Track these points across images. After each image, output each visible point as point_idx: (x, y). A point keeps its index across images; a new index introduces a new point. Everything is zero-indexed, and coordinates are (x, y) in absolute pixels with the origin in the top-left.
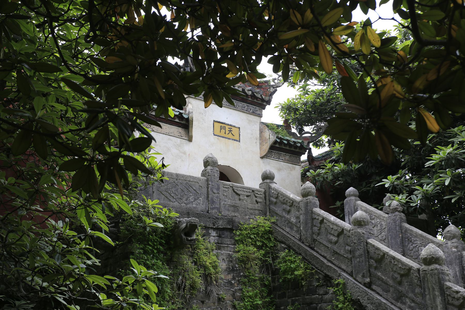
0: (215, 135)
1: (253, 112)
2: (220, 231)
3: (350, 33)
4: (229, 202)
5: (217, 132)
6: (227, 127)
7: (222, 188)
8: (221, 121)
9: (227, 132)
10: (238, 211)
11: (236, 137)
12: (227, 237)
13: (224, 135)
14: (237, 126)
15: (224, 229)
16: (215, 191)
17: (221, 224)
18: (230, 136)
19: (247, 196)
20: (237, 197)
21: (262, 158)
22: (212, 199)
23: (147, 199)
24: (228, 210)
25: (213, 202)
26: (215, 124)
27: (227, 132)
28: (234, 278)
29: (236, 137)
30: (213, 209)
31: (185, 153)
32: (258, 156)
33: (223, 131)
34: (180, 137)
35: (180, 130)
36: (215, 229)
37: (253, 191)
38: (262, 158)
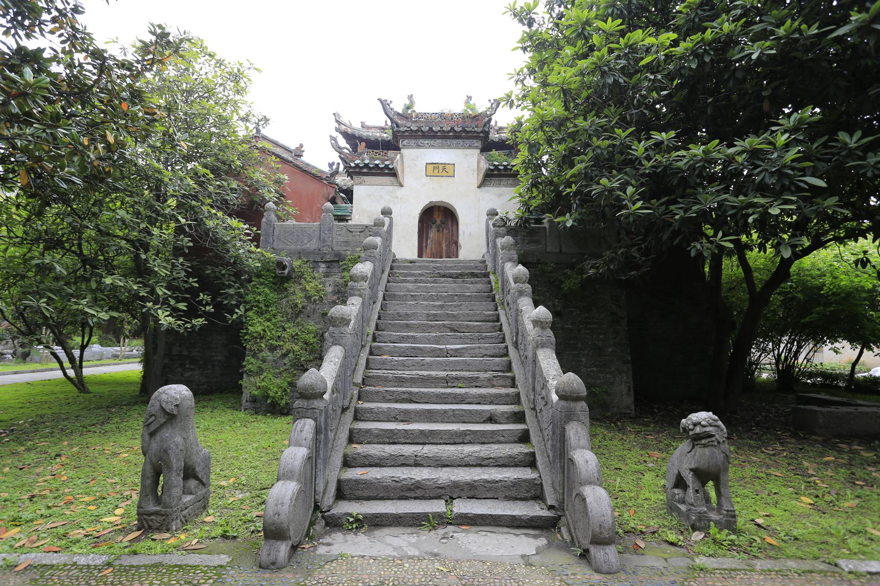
0: (427, 176)
1: (470, 146)
2: (330, 263)
3: (753, 25)
4: (341, 239)
5: (430, 172)
6: (441, 167)
7: (335, 228)
8: (434, 162)
9: (441, 170)
10: (350, 246)
11: (451, 174)
12: (334, 268)
13: (438, 174)
14: (451, 163)
15: (331, 261)
16: (326, 232)
17: (328, 258)
18: (444, 173)
19: (360, 232)
20: (350, 234)
21: (479, 187)
22: (324, 239)
23: (780, 209)
24: (341, 246)
25: (324, 241)
26: (428, 166)
27: (441, 170)
28: (338, 298)
29: (451, 174)
30: (324, 246)
31: (397, 197)
32: (476, 185)
33: (436, 170)
34: (393, 185)
35: (392, 178)
36: (324, 262)
37: (367, 227)
38: (479, 187)
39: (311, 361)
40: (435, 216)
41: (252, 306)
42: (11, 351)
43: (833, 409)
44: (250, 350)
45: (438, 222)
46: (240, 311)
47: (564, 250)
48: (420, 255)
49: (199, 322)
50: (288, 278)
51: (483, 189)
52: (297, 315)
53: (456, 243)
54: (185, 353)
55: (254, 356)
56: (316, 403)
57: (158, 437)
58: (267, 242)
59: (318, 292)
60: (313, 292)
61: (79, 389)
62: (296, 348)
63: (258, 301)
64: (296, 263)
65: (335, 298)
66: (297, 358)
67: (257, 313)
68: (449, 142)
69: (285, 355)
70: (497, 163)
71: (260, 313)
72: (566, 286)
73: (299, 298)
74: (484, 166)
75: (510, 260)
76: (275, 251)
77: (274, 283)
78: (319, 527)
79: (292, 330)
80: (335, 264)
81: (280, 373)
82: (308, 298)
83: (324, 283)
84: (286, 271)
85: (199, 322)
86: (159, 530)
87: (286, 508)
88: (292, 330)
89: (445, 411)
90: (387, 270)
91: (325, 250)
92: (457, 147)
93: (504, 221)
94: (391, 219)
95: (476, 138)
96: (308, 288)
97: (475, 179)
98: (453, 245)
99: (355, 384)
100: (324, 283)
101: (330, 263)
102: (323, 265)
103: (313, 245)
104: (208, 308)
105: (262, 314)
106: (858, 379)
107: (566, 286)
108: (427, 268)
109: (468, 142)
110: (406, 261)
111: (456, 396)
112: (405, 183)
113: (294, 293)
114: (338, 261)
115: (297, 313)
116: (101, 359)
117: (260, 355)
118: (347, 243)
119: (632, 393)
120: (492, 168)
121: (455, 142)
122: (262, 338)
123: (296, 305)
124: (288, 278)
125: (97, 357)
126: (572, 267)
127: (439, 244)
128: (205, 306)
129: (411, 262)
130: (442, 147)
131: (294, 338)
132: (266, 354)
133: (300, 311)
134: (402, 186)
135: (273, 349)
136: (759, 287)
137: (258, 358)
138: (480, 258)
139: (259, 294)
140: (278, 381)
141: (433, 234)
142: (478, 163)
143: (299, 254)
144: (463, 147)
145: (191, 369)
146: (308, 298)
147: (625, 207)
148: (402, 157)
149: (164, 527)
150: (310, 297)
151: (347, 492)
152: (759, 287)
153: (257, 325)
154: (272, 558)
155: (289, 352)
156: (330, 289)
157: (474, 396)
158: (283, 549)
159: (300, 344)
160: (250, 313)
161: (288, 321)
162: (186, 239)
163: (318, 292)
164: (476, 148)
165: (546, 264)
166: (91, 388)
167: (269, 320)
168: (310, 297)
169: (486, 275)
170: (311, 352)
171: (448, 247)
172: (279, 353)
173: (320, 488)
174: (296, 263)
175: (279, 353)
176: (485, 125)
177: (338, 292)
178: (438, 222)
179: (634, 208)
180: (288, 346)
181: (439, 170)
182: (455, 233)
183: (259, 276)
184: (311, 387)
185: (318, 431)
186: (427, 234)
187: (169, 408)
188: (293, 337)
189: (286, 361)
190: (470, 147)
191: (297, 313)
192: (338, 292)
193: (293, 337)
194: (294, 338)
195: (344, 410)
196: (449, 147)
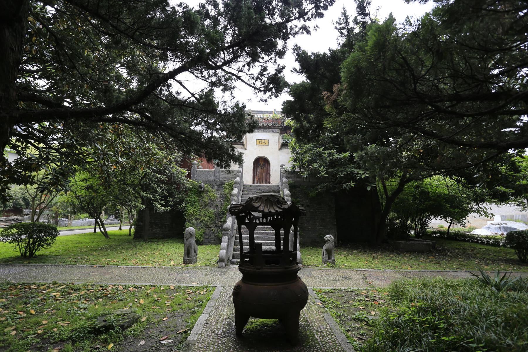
2: (219, 186)
4: (223, 176)
7: (221, 172)
17: (218, 183)
21: (279, 150)
32: (278, 149)
33: (261, 143)
35: (241, 146)
38: (279, 150)
39: (211, 224)
40: (260, 162)
41: (188, 203)
42: (47, 221)
43: (417, 242)
44: (188, 220)
45: (262, 165)
46: (184, 204)
47: (311, 181)
48: (253, 183)
49: (169, 208)
50: (203, 192)
51: (281, 151)
52: (206, 206)
53: (269, 174)
54: (153, 221)
55: (189, 222)
56: (228, 232)
57: (188, 240)
58: (194, 177)
59: (214, 197)
60: (212, 197)
61: (106, 237)
62: (206, 219)
63: (191, 201)
64: (206, 186)
65: (221, 199)
66: (206, 223)
67: (190, 205)
68: (266, 130)
69: (201, 222)
70: (286, 140)
71: (192, 205)
72: (310, 195)
73: (207, 200)
74: (281, 141)
75: (286, 188)
76: (197, 180)
77: (197, 193)
78: (229, 263)
79: (204, 212)
80: (221, 186)
81: (199, 229)
82: (210, 199)
83: (216, 194)
84: (202, 189)
85: (169, 208)
86: (189, 263)
87: (224, 255)
88: (204, 212)
89: (262, 237)
90: (242, 189)
91: (217, 180)
92: (270, 132)
93: (286, 171)
94: (243, 168)
95: (278, 128)
96: (210, 195)
97: (277, 146)
98: (268, 181)
99: (235, 230)
100: (216, 194)
101: (219, 186)
102: (216, 186)
103: (212, 178)
104: (171, 203)
105: (192, 205)
106: (428, 232)
107: (310, 195)
108: (257, 189)
109: (274, 130)
110: (249, 185)
111: (266, 233)
112: (247, 148)
113: (205, 198)
114: (222, 185)
115: (206, 205)
116: (90, 225)
117: (191, 222)
118: (225, 177)
119: (336, 237)
120: (285, 142)
121: (269, 130)
122: (192, 215)
123: (206, 202)
124: (203, 192)
125: (89, 224)
126: (313, 187)
127: (262, 174)
128: (170, 202)
129: (251, 186)
130: (263, 132)
131: (205, 215)
132: (194, 221)
133: (207, 205)
134: (246, 149)
135: (196, 219)
136: (390, 194)
137: (190, 223)
138: (278, 184)
139: (191, 198)
140: (199, 232)
141: (259, 170)
142: (279, 139)
143: (206, 182)
144: (272, 132)
145: (156, 228)
146: (210, 199)
147: (320, 173)
148: (246, 137)
149: (190, 263)
150: (211, 199)
151: (235, 257)
152: (390, 194)
153: (191, 210)
154: (221, 266)
155: (203, 220)
156: (219, 196)
157: (271, 233)
158: (224, 264)
159: (207, 217)
160: (188, 205)
161: (202, 208)
162: (164, 177)
163: (214, 197)
164: (278, 133)
165: (303, 186)
166: (110, 237)
167: (195, 208)
168: (211, 199)
169: (279, 192)
170: (212, 220)
171: (266, 175)
172: (199, 221)
173: (229, 254)
174: (206, 186)
175: (199, 221)
176: (282, 123)
177: (222, 197)
178: (262, 165)
179: (322, 174)
180: (203, 218)
181: (262, 143)
182: (269, 169)
183: (191, 190)
184: (227, 228)
185: (229, 239)
186: (257, 170)
187: (191, 233)
188: (204, 214)
189: (202, 224)
190: (275, 132)
191: (206, 205)
192: (222, 197)
193: (204, 214)
194: (205, 215)
195: (232, 236)
196: (266, 132)
